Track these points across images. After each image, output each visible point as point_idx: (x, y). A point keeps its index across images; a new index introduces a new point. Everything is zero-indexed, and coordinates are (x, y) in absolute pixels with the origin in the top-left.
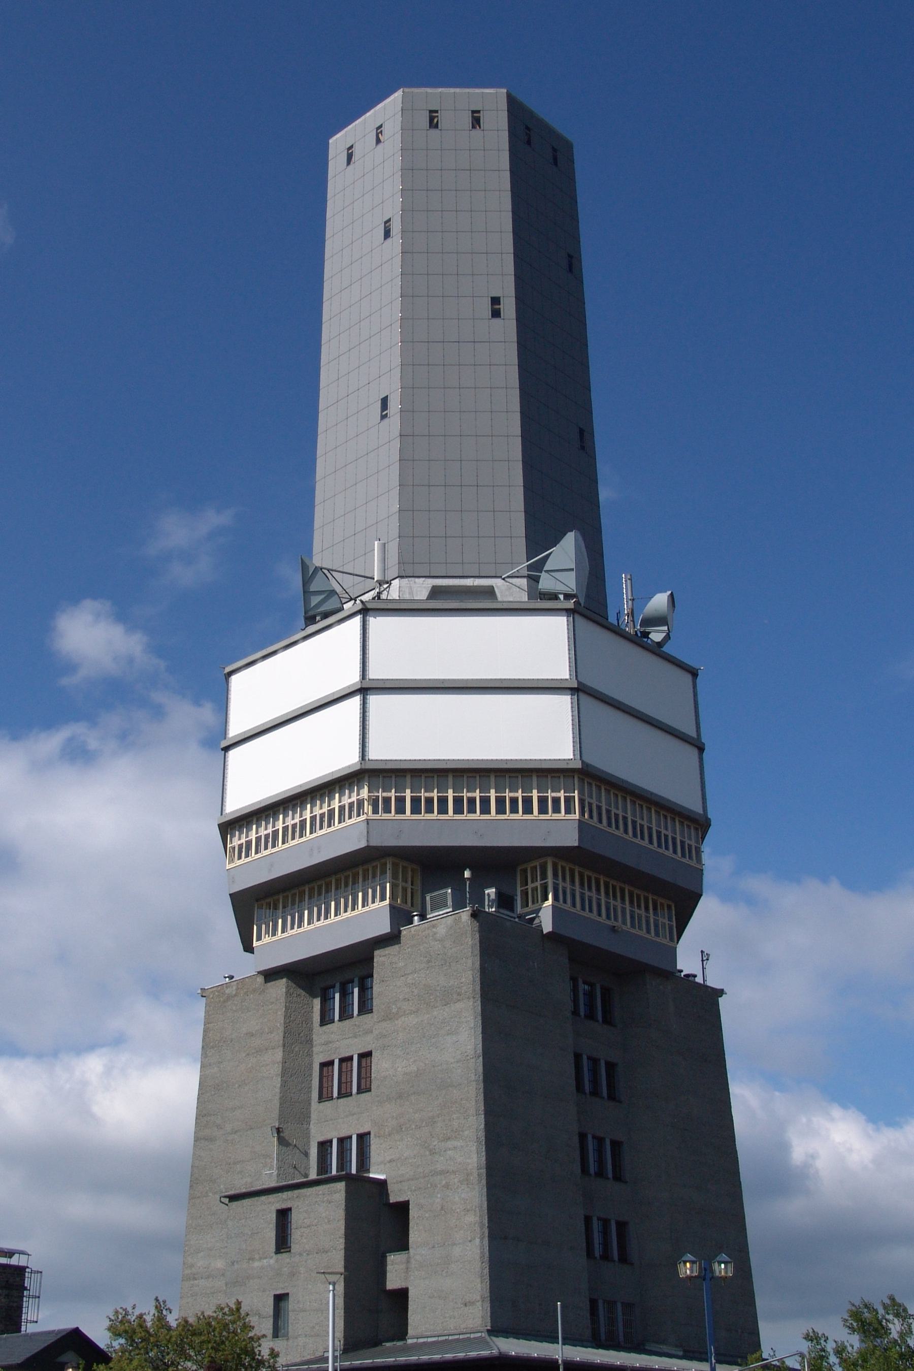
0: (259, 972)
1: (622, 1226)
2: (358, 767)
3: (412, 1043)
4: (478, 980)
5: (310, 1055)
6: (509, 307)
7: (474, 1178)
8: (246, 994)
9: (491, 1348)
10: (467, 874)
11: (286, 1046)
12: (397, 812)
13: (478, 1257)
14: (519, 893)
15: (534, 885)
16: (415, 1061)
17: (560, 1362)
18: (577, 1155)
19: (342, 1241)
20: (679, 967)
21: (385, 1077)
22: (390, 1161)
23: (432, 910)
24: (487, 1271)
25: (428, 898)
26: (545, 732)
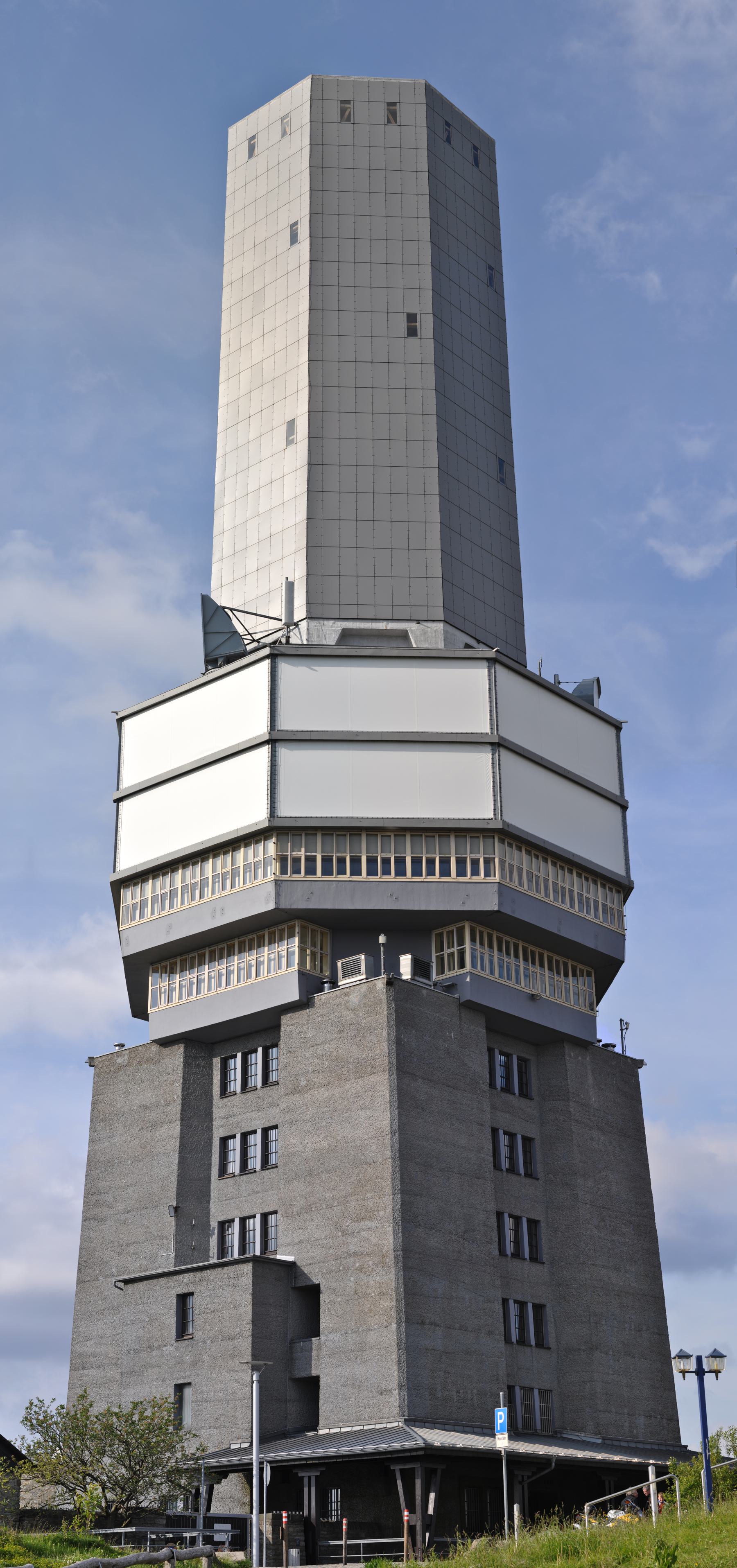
0: (154, 1041)
1: (539, 1308)
2: (266, 824)
3: (322, 1118)
4: (394, 1052)
5: (210, 1129)
6: (426, 325)
7: (390, 1260)
8: (139, 1063)
9: (412, 1438)
10: (382, 939)
11: (185, 1120)
12: (441, 875)
13: (394, 1343)
14: (434, 959)
15: (450, 951)
16: (326, 1137)
17: (503, 1453)
18: (495, 1235)
19: (249, 1327)
20: (599, 1037)
21: (293, 1154)
22: (299, 1242)
23: (344, 976)
24: (403, 1358)
25: (339, 964)
26: (462, 790)
